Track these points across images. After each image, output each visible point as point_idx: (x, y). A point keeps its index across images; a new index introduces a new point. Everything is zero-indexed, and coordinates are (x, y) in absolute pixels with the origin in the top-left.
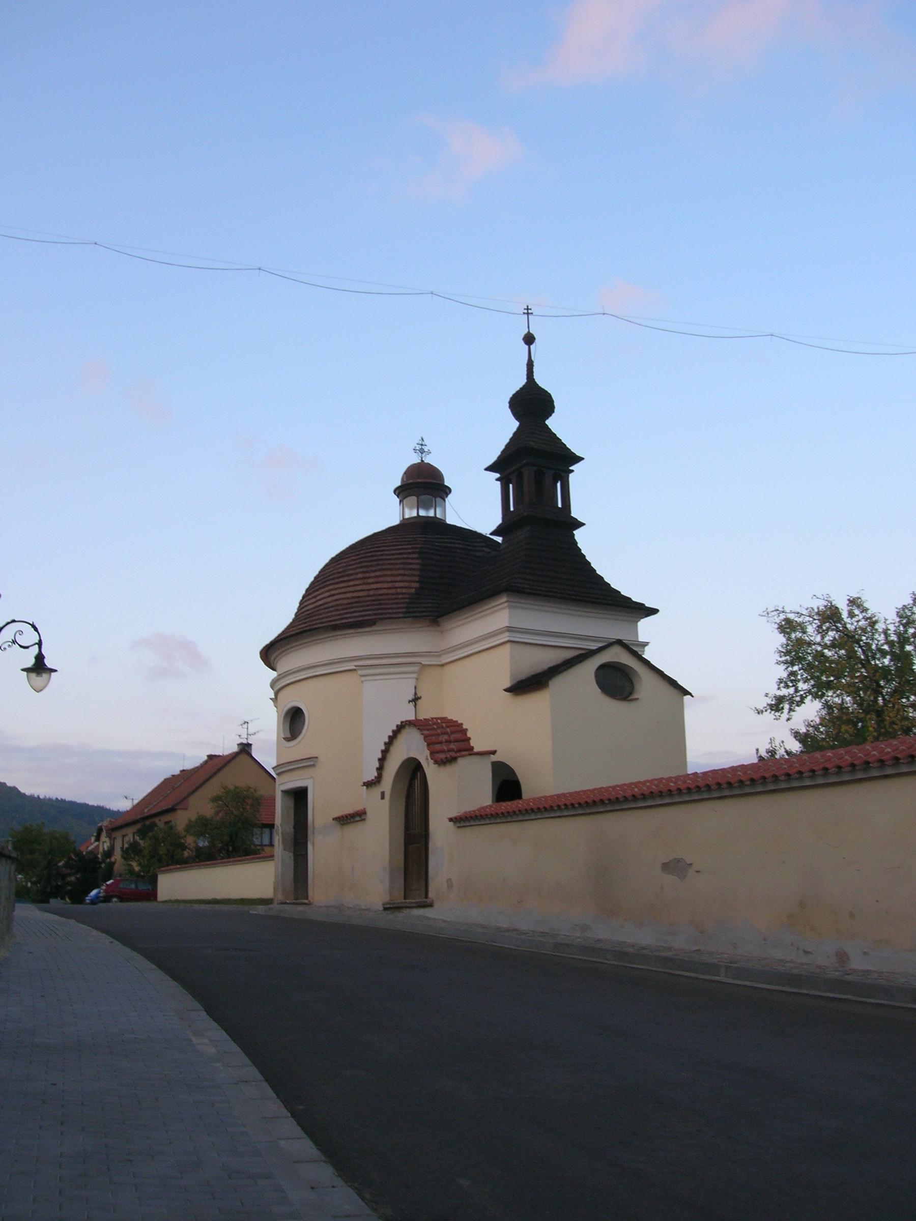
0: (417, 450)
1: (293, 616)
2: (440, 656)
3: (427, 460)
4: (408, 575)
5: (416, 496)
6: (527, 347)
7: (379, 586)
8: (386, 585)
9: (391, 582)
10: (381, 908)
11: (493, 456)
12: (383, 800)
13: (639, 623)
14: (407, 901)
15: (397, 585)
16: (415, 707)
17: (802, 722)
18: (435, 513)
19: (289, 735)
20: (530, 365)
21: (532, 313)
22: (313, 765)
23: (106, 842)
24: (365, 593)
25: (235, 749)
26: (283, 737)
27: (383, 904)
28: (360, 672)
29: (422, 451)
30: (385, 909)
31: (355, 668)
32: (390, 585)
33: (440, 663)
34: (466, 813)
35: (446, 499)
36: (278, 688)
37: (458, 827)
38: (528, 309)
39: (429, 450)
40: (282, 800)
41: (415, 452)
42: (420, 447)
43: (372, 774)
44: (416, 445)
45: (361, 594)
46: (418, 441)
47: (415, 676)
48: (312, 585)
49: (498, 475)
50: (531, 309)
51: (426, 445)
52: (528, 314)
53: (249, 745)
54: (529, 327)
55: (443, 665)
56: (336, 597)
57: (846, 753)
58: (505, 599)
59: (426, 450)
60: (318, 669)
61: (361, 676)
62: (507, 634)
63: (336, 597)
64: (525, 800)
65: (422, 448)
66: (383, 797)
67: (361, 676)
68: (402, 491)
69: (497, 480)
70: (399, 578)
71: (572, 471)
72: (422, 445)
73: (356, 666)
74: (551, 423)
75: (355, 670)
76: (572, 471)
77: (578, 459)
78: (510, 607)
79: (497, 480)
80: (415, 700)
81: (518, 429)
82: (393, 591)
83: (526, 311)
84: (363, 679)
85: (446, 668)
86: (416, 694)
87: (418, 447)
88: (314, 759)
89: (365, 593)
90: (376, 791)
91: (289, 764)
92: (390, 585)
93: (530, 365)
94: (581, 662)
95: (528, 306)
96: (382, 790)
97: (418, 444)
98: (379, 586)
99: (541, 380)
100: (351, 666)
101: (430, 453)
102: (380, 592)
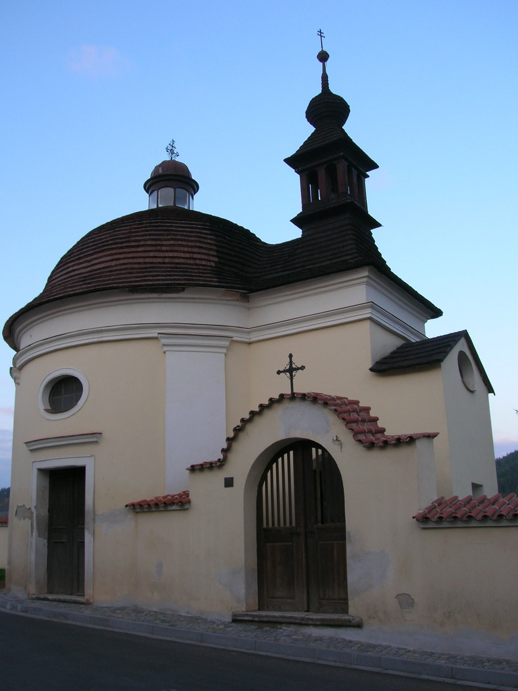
0: (168, 149)
2: (249, 333)
3: (177, 159)
4: (205, 248)
5: (173, 188)
6: (321, 64)
7: (175, 254)
8: (182, 255)
9: (188, 252)
11: (292, 151)
12: (229, 489)
13: (426, 324)
14: (263, 613)
15: (195, 256)
18: (189, 208)
19: (49, 408)
20: (325, 79)
21: (324, 37)
22: (96, 442)
24: (160, 260)
26: (44, 408)
27: (234, 615)
28: (164, 341)
29: (172, 152)
30: (234, 621)
31: (156, 335)
32: (188, 255)
33: (248, 340)
34: (157, 498)
35: (194, 197)
38: (320, 32)
40: (38, 480)
41: (168, 151)
42: (171, 148)
44: (169, 145)
45: (155, 260)
46: (169, 141)
47: (225, 351)
48: (71, 253)
50: (323, 33)
51: (175, 148)
52: (321, 36)
54: (322, 47)
55: (250, 343)
56: (121, 262)
58: (366, 274)
60: (104, 334)
61: (164, 345)
62: (369, 310)
63: (121, 262)
64: (12, 486)
65: (172, 149)
66: (229, 483)
67: (164, 345)
70: (195, 250)
71: (368, 176)
72: (172, 146)
73: (159, 333)
75: (156, 338)
76: (368, 176)
77: (374, 166)
78: (368, 284)
80: (291, 370)
81: (315, 130)
82: (192, 262)
83: (319, 34)
84: (165, 349)
85: (252, 346)
86: (291, 362)
87: (170, 148)
88: (98, 435)
89: (160, 260)
90: (218, 477)
91: (57, 439)
92: (188, 255)
93: (325, 79)
95: (320, 30)
96: (229, 476)
97: (169, 144)
98: (175, 254)
99: (334, 89)
100: (154, 333)
101: (179, 155)
102: (177, 261)
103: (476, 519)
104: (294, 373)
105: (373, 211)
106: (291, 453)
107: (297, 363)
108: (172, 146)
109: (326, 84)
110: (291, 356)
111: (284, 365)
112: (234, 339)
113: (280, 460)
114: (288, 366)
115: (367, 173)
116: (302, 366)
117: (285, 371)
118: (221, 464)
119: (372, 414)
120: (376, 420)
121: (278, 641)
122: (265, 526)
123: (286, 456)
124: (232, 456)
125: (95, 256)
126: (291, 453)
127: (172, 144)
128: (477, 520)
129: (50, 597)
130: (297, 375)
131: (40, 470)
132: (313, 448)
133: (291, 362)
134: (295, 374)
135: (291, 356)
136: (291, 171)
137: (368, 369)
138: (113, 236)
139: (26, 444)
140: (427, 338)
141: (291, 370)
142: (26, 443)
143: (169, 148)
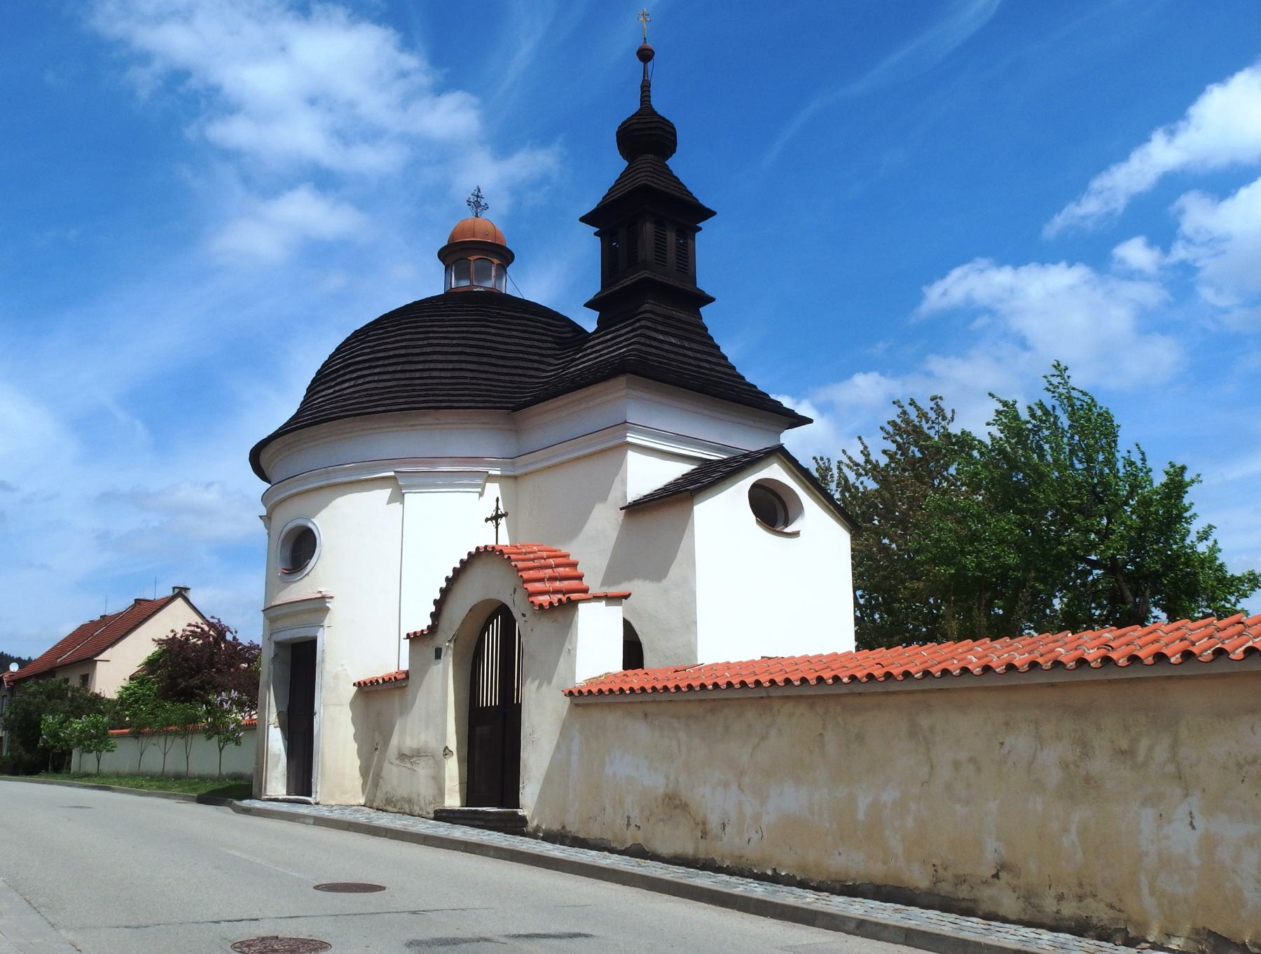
1: (266, 437)
10: (432, 815)
16: (497, 528)
17: (242, 744)
19: (289, 567)
20: (646, 88)
23: (6, 696)
25: (170, 593)
31: (392, 474)
33: (512, 474)
35: (508, 269)
36: (272, 505)
37: (577, 705)
39: (486, 204)
42: (476, 199)
43: (424, 623)
47: (480, 490)
49: (598, 229)
53: (186, 589)
57: (731, 676)
59: (482, 204)
68: (444, 255)
69: (596, 234)
72: (478, 196)
74: (674, 163)
76: (700, 229)
77: (708, 214)
79: (596, 234)
86: (497, 508)
93: (646, 88)
94: (738, 472)
99: (660, 104)
105: (704, 283)
108: (478, 196)
109: (647, 96)
111: (491, 512)
115: (698, 225)
118: (433, 629)
119: (580, 569)
120: (580, 578)
121: (162, 891)
125: (505, 370)
136: (707, 205)
138: (475, 321)
140: (747, 452)
143: (472, 200)
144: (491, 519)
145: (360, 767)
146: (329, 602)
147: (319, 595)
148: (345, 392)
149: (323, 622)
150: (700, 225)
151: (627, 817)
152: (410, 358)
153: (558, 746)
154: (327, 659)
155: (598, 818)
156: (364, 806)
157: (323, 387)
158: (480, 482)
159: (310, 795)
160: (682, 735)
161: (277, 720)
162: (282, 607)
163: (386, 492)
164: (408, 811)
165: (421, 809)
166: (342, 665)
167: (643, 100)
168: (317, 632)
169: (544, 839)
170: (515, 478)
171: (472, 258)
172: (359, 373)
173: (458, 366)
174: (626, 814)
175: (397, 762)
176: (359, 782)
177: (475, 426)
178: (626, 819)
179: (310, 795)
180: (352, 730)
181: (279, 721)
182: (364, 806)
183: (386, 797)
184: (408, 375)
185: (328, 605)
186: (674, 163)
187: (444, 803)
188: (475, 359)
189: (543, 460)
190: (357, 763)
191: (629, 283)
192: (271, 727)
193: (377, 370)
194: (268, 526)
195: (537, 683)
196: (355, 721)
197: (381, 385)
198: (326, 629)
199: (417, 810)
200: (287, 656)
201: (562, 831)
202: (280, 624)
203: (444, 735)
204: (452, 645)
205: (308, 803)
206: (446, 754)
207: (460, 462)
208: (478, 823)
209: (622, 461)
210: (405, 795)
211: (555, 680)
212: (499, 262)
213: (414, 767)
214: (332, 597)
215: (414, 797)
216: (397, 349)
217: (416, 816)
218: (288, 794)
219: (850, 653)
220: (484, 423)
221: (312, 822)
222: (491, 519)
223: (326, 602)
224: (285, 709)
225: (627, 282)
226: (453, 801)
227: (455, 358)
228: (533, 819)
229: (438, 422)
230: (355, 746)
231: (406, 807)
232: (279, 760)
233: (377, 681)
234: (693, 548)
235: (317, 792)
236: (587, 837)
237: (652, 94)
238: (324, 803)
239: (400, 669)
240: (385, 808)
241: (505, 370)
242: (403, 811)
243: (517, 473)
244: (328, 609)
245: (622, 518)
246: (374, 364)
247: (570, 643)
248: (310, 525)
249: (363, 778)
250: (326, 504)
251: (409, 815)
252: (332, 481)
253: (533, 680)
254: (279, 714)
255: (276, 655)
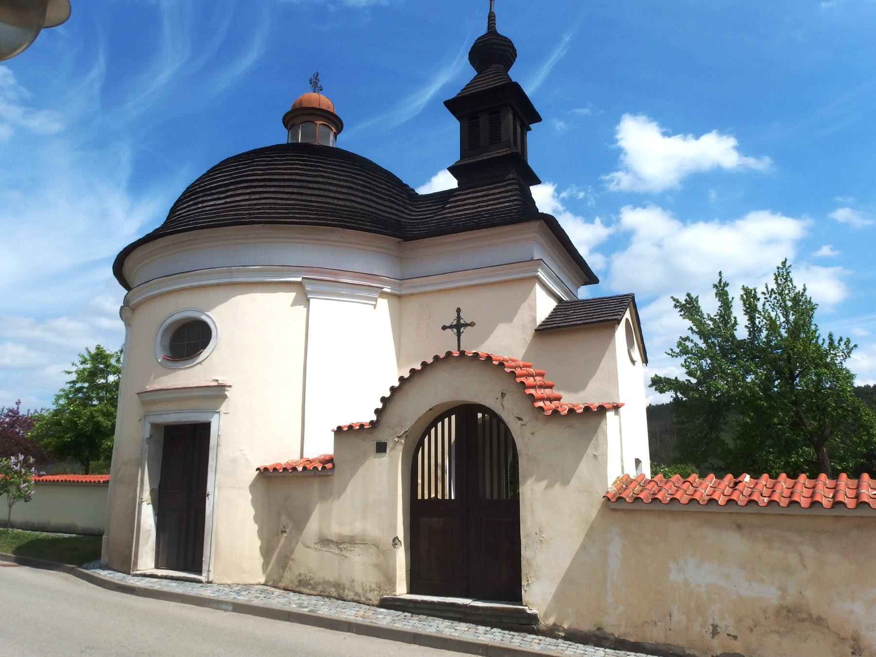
20: (491, 18)
31: (300, 279)
33: (398, 293)
72: (316, 79)
93: (491, 18)
99: (502, 29)
103: (848, 507)
104: (462, 329)
106: (453, 417)
107: (466, 319)
108: (316, 79)
110: (458, 310)
111: (451, 320)
112: (384, 290)
113: (440, 424)
114: (456, 321)
116: (472, 322)
117: (451, 327)
122: (420, 497)
123: (446, 420)
124: (386, 418)
125: (383, 208)
126: (453, 417)
127: (316, 75)
128: (803, 508)
129: (160, 572)
130: (466, 332)
131: (154, 426)
132: (478, 414)
133: (459, 318)
134: (463, 330)
135: (458, 310)
137: (290, 306)
139: (139, 395)
141: (458, 326)
142: (138, 394)
144: (466, 325)
145: (261, 548)
146: (228, 391)
147: (215, 384)
148: (242, 203)
149: (219, 408)
150: (531, 126)
151: (712, 625)
152: (305, 184)
153: (583, 547)
154: (223, 442)
155: (659, 624)
156: (264, 584)
157: (209, 198)
158: (376, 296)
159: (200, 572)
160: (808, 550)
161: (150, 497)
162: (169, 391)
163: (292, 295)
164: (335, 594)
165: (356, 594)
166: (241, 450)
167: (490, 26)
168: (212, 418)
169: (566, 638)
170: (399, 297)
171: (318, 122)
172: (253, 190)
173: (348, 197)
174: (711, 622)
175: (318, 546)
176: (259, 561)
177: (371, 248)
178: (711, 628)
179: (200, 572)
180: (251, 512)
181: (151, 498)
182: (264, 584)
183: (299, 578)
184: (304, 198)
185: (226, 393)
186: (514, 74)
187: (395, 591)
188: (361, 195)
189: (412, 287)
190: (257, 543)
191: (496, 155)
192: (144, 505)
193: (272, 189)
194: (128, 324)
195: (544, 483)
196: (254, 503)
197: (279, 202)
198: (222, 416)
199: (350, 595)
200: (161, 437)
201: (598, 633)
202: (154, 408)
203: (394, 528)
204: (403, 441)
205: (199, 582)
206: (396, 544)
207: (360, 277)
208: (451, 615)
209: (529, 293)
210: (331, 579)
211: (574, 482)
212: (335, 131)
213: (344, 553)
214: (231, 386)
215: (345, 581)
216: (292, 175)
217: (349, 601)
218: (157, 567)
219: (212, 418)
220: (379, 247)
221: (231, 608)
222: (466, 325)
223: (225, 390)
224: (156, 487)
225: (485, 157)
226: (401, 590)
227: (344, 190)
228: (546, 616)
229: (343, 240)
230: (255, 527)
231: (333, 591)
232: (150, 535)
233: (294, 469)
234: (615, 368)
235: (209, 571)
236: (640, 641)
237: (496, 22)
238: (217, 582)
239: (306, 456)
240: (297, 589)
241: (383, 208)
242: (327, 594)
243: (403, 292)
244: (225, 397)
245: (531, 338)
246: (269, 184)
247: (596, 448)
248: (204, 318)
249: (264, 558)
250: (225, 300)
251: (337, 599)
252: (234, 280)
253: (538, 480)
254: (152, 491)
255: (151, 436)
